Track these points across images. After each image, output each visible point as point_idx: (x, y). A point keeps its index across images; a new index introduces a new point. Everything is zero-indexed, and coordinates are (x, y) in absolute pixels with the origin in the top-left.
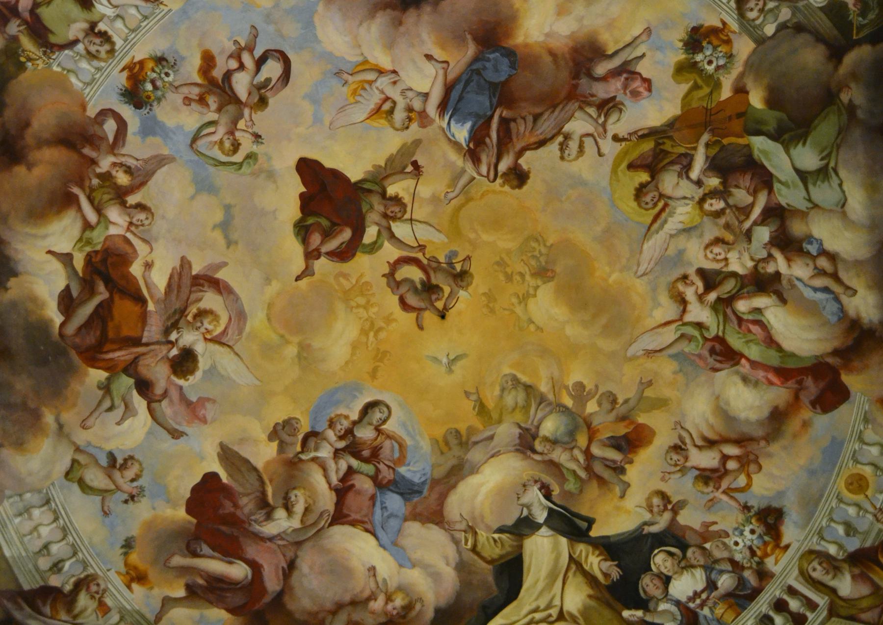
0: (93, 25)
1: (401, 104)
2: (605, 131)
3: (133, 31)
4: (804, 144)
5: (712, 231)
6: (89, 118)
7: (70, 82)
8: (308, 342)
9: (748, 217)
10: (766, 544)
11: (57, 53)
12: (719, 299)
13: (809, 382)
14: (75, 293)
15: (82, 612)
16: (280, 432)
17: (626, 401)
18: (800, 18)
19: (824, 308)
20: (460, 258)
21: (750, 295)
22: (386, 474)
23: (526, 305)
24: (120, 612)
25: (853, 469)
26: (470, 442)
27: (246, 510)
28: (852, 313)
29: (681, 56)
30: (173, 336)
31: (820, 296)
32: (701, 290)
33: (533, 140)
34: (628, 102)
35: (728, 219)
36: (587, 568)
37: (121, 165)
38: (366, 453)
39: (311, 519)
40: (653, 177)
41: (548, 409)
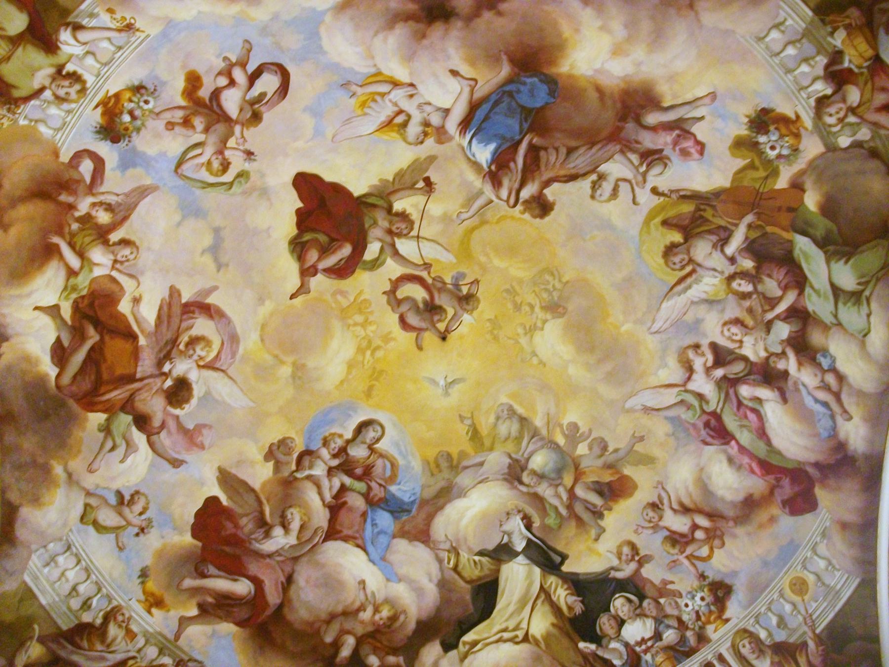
0: (60, 69)
1: (417, 117)
2: (645, 181)
3: (105, 64)
4: (846, 262)
5: (733, 310)
6: (63, 163)
7: (41, 133)
8: (303, 361)
9: (773, 308)
10: (711, 612)
11: (22, 107)
12: (725, 378)
13: (786, 482)
14: (66, 343)
15: (114, 640)
16: (275, 452)
17: (616, 451)
18: (878, 144)
19: (820, 420)
20: (469, 280)
21: (756, 384)
22: (378, 492)
23: (532, 336)
24: (144, 636)
25: (797, 571)
26: (461, 466)
27: (246, 530)
28: (842, 435)
29: (744, 131)
30: (166, 368)
31: (818, 408)
32: (710, 363)
33: (562, 172)
34: (675, 157)
35: (753, 303)
36: (554, 599)
37: (101, 204)
38: (359, 471)
39: (308, 534)
40: (686, 240)
41: (539, 444)
